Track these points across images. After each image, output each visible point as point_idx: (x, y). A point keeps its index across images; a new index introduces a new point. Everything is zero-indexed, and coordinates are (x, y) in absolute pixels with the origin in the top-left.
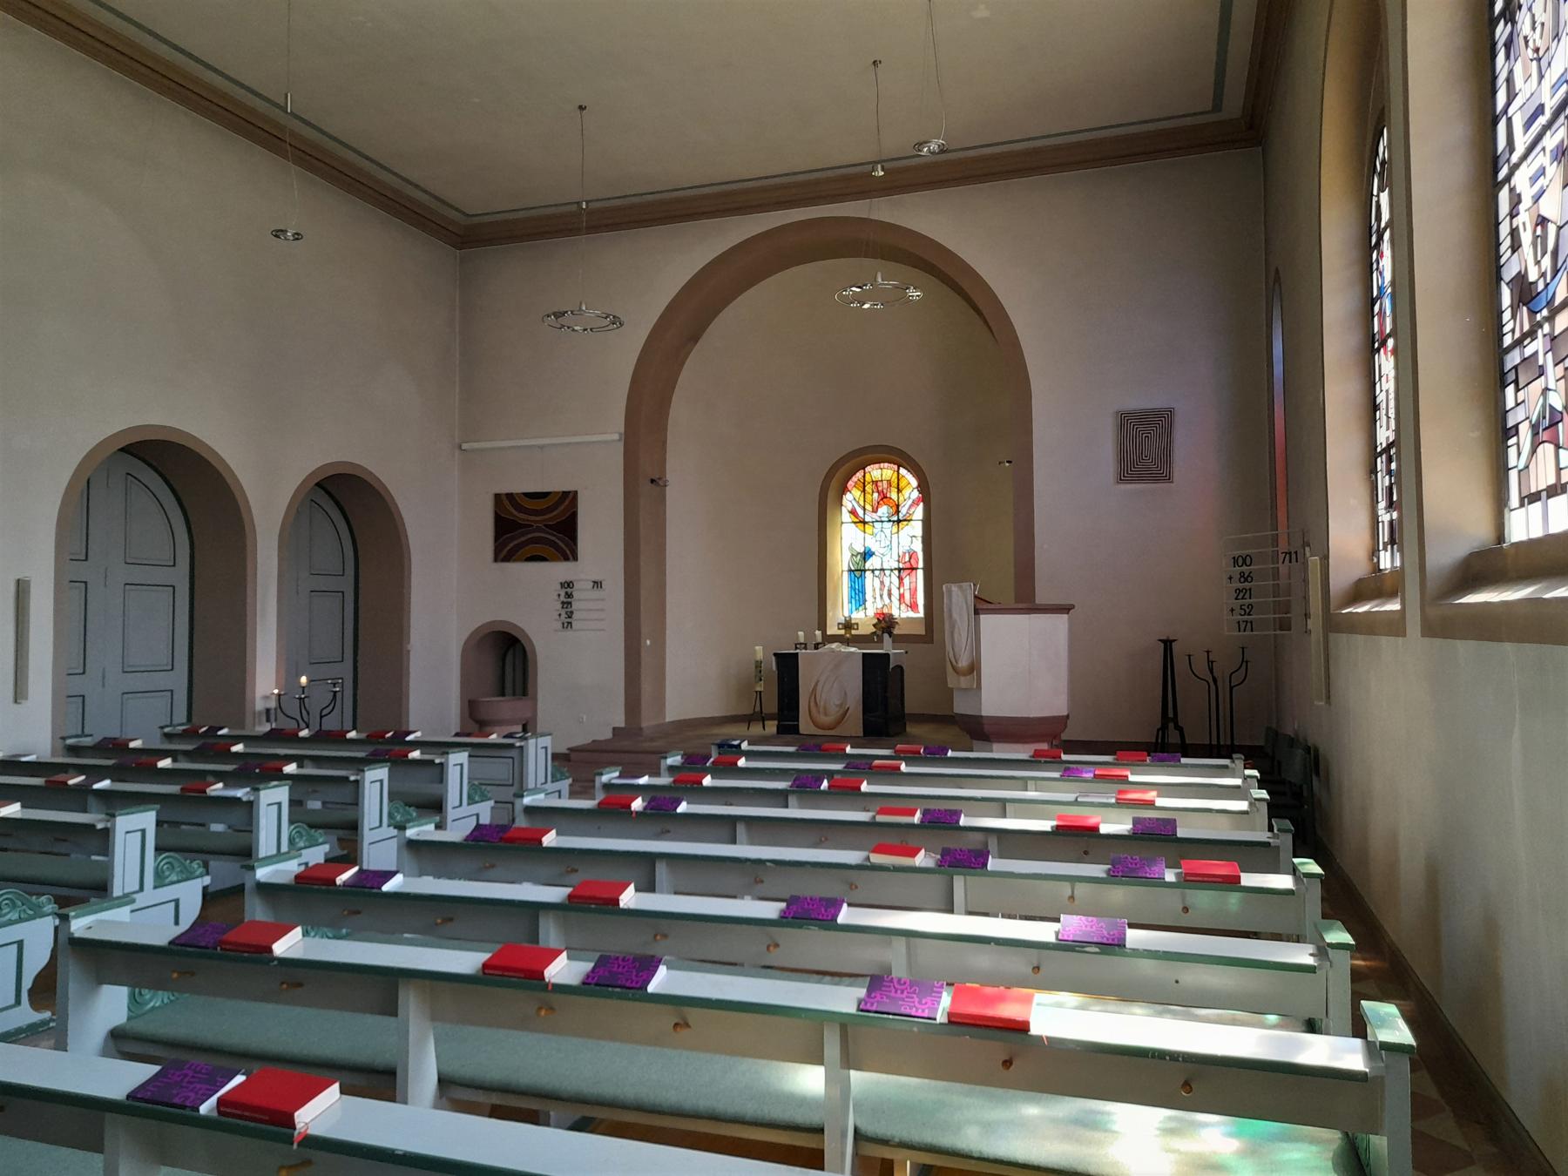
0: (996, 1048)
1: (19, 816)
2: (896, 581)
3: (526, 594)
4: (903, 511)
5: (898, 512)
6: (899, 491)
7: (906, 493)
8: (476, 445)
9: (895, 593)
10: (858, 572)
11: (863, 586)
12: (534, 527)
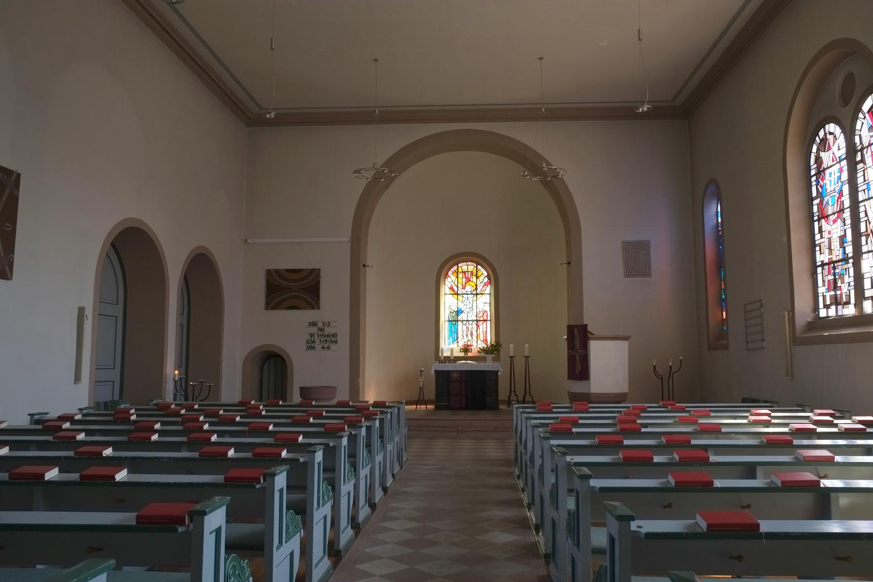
0: (805, 499)
1: (9, 454)
2: (475, 327)
3: (288, 329)
4: (479, 289)
5: (476, 289)
6: (477, 278)
7: (481, 279)
8: (257, 241)
9: (475, 333)
10: (454, 321)
11: (457, 330)
12: (291, 289)
